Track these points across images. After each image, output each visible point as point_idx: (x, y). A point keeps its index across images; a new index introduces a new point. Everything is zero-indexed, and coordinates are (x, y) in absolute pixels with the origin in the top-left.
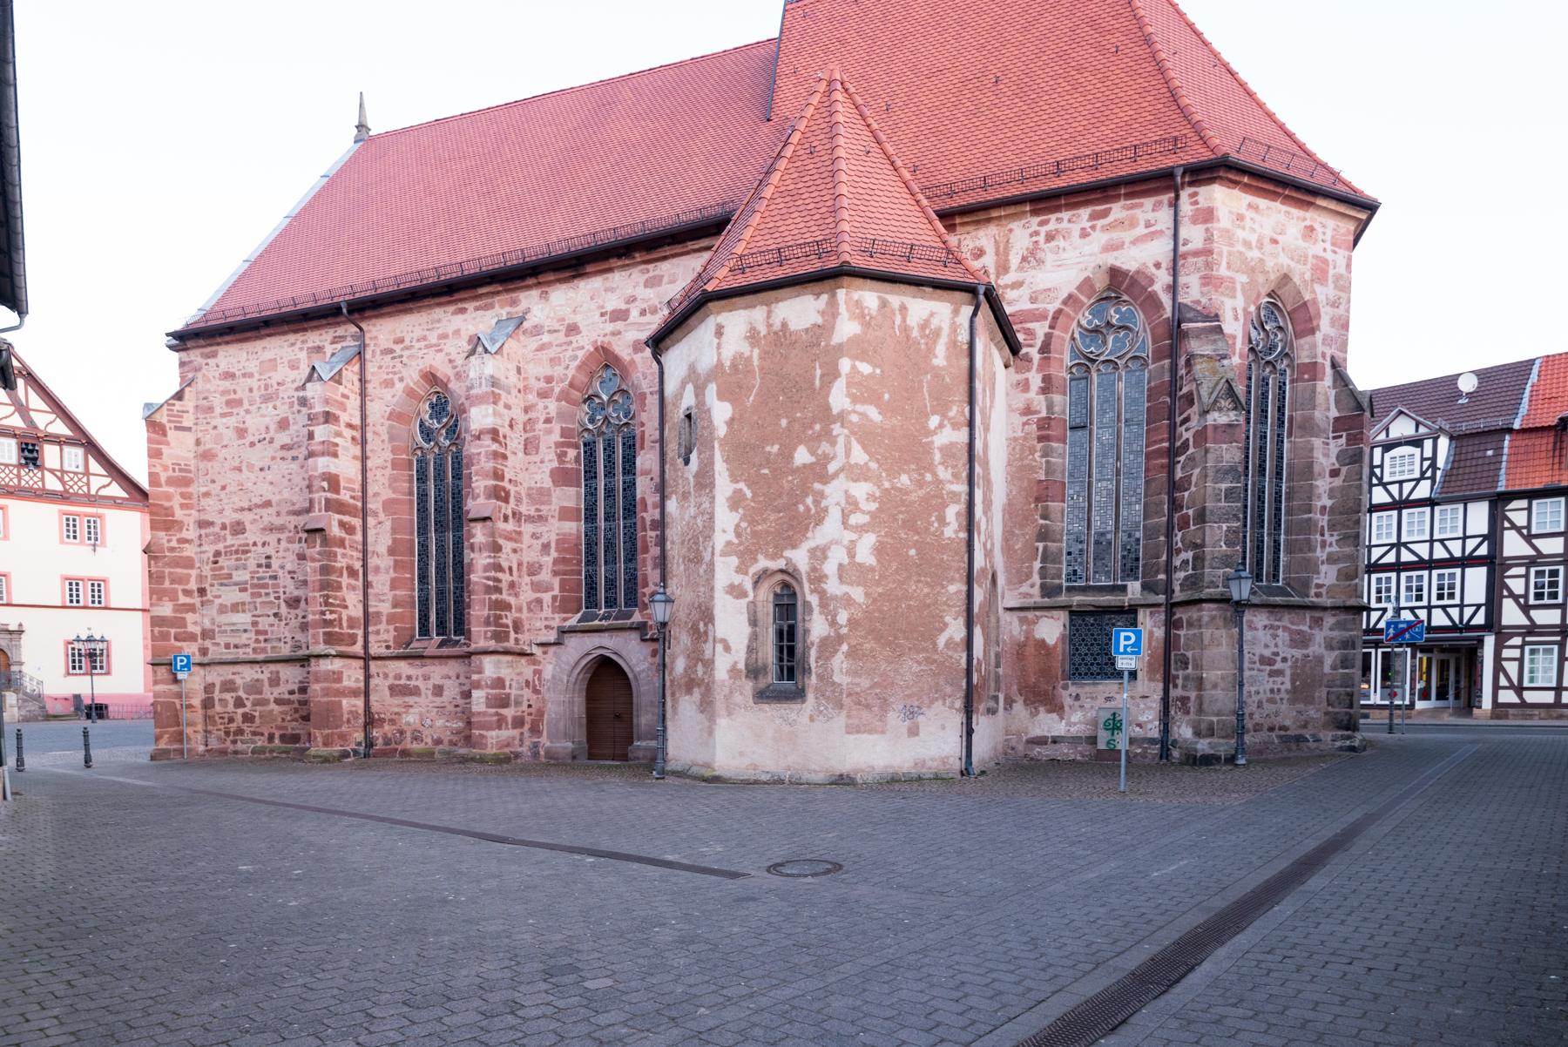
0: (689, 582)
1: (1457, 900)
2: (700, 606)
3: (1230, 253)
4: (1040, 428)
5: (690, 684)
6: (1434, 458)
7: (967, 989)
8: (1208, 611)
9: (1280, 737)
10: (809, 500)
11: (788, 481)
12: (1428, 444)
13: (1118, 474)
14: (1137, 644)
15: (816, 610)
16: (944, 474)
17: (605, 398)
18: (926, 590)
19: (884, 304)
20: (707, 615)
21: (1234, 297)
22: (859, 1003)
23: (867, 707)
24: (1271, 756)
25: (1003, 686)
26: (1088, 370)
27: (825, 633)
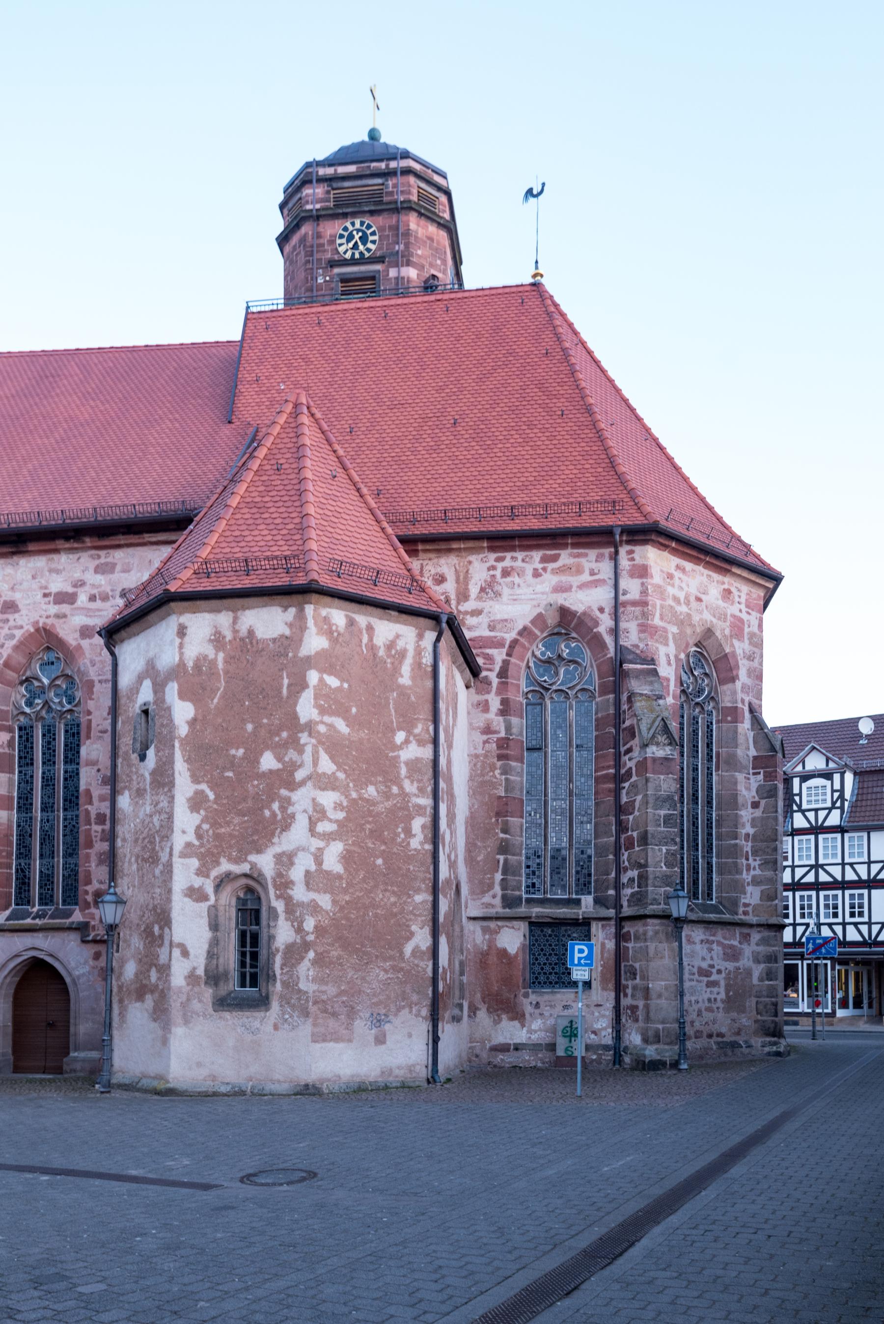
0: (141, 882)
1: (842, 1181)
2: (155, 908)
3: (662, 607)
4: (499, 747)
5: (141, 991)
6: (842, 790)
7: (444, 1272)
8: (653, 926)
9: (718, 1043)
10: (276, 806)
11: (254, 786)
12: (837, 777)
13: (571, 795)
14: (589, 957)
15: (282, 916)
16: (410, 787)
17: (46, 681)
18: (393, 899)
19: (351, 623)
20: (164, 918)
21: (667, 645)
22: (348, 1288)
23: (333, 1016)
24: (709, 1062)
25: (467, 994)
26: (542, 697)
27: (290, 940)
